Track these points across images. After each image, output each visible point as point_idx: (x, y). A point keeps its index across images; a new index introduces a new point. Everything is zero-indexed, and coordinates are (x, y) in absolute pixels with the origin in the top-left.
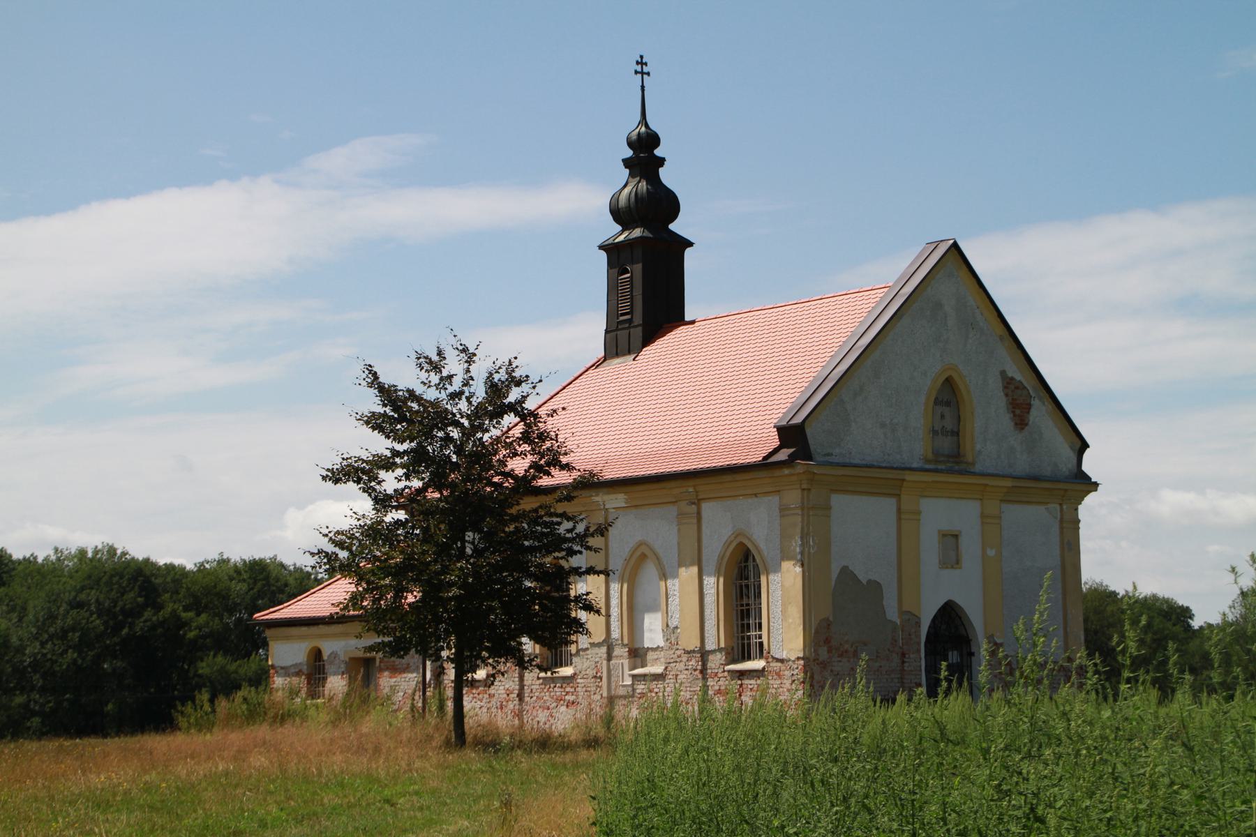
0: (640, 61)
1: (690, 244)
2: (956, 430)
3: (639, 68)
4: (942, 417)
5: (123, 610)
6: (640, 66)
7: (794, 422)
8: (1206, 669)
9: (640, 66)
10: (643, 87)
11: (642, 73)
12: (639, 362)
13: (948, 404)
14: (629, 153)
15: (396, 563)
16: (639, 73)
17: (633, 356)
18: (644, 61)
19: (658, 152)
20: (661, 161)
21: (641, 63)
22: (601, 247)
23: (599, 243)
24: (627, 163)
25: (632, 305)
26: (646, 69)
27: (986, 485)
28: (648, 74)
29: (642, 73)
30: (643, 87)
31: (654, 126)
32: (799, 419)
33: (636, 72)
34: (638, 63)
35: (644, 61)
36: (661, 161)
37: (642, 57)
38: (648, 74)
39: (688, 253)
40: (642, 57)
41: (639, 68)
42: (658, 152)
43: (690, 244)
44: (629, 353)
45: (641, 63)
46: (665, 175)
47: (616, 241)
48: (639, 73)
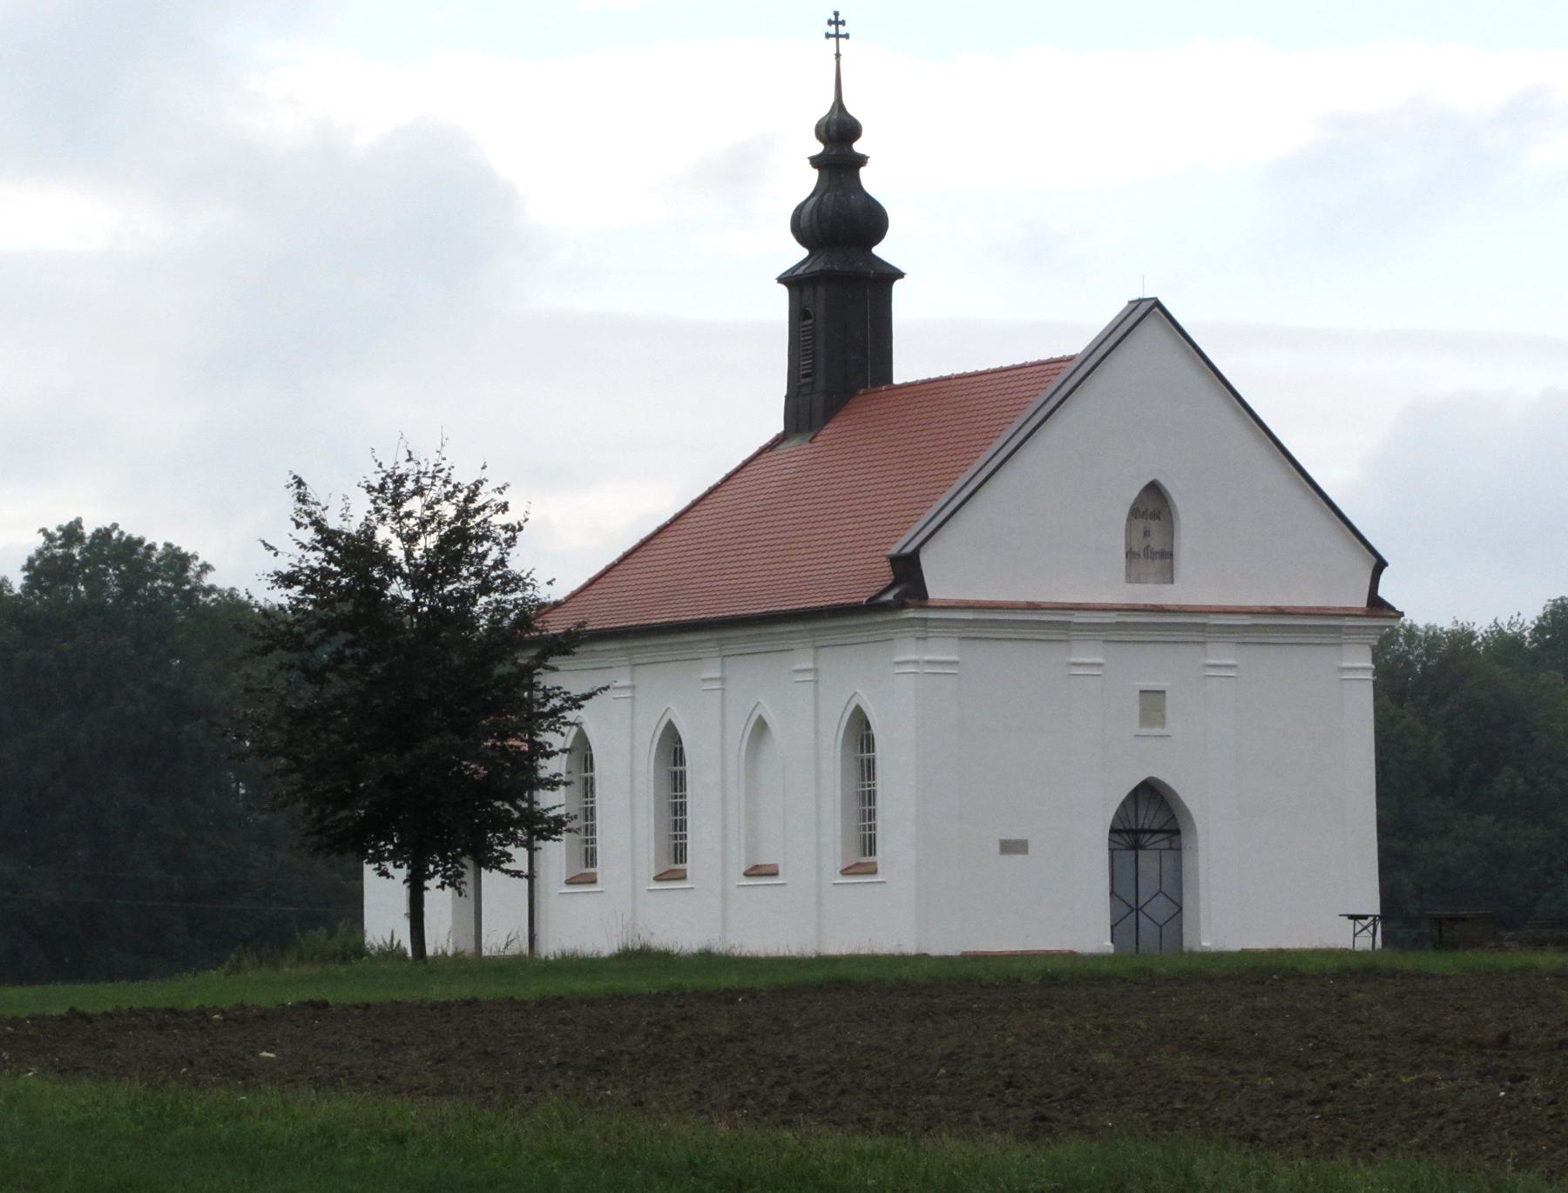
0: (833, 19)
1: (900, 275)
2: (1167, 549)
3: (832, 30)
4: (1146, 533)
5: (503, 607)
6: (833, 26)
7: (904, 551)
8: (185, 568)
9: (833, 26)
10: (838, 55)
11: (837, 36)
12: (817, 444)
13: (1155, 516)
14: (818, 148)
15: (542, 824)
16: (832, 36)
17: (810, 435)
18: (840, 19)
19: (858, 147)
20: (861, 160)
21: (836, 22)
22: (781, 280)
23: (779, 274)
24: (816, 162)
25: (813, 365)
26: (842, 30)
27: (926, 619)
28: (847, 36)
29: (837, 36)
30: (838, 55)
31: (853, 108)
32: (909, 549)
33: (828, 36)
34: (830, 23)
35: (840, 19)
36: (861, 160)
37: (836, 14)
38: (847, 36)
39: (898, 287)
40: (836, 14)
41: (832, 30)
42: (858, 147)
43: (900, 275)
44: (810, 429)
45: (836, 22)
46: (869, 179)
47: (796, 273)
48: (832, 36)
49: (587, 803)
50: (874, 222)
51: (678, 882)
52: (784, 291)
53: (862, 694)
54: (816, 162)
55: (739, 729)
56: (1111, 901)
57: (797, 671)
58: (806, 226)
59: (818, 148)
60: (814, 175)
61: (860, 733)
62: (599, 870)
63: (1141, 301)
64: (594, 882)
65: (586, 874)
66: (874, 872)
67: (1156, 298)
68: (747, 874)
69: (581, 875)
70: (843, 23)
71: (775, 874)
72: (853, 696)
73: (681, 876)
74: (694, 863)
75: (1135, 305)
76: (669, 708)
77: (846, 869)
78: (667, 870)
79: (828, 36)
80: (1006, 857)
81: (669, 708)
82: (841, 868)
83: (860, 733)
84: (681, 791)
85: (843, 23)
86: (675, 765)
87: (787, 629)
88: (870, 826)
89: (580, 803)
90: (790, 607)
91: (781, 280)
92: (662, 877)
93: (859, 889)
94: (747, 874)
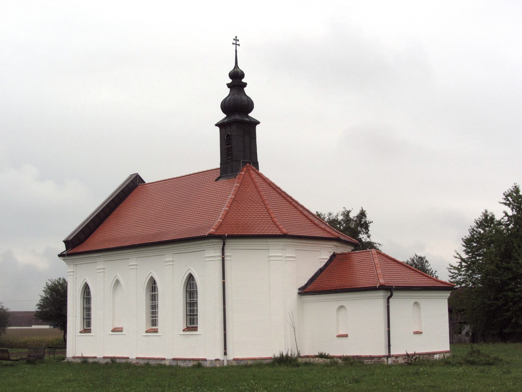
1: (258, 123)
3: (234, 42)
6: (235, 41)
9: (235, 41)
11: (236, 44)
18: (237, 39)
20: (245, 85)
21: (236, 40)
22: (216, 125)
24: (229, 85)
26: (238, 43)
29: (236, 44)
33: (233, 44)
34: (234, 40)
35: (237, 39)
36: (245, 85)
37: (236, 37)
38: (239, 45)
39: (258, 127)
40: (236, 37)
41: (234, 42)
43: (258, 123)
45: (236, 40)
46: (247, 90)
49: (153, 303)
50: (249, 106)
51: (155, 333)
52: (218, 129)
53: (119, 276)
54: (229, 85)
55: (110, 283)
56: (450, 346)
57: (97, 269)
58: (226, 107)
59: (230, 81)
60: (228, 90)
61: (152, 285)
62: (93, 327)
63: (133, 175)
64: (157, 332)
65: (153, 329)
66: (90, 332)
67: (137, 173)
68: (112, 331)
69: (151, 329)
70: (238, 40)
71: (122, 331)
72: (150, 273)
73: (156, 331)
74: (160, 326)
75: (131, 175)
76: (85, 279)
77: (81, 332)
78: (149, 329)
79: (233, 44)
80: (122, 327)
81: (85, 279)
82: (183, 329)
83: (152, 285)
84: (89, 304)
85: (238, 40)
86: (153, 292)
87: (273, 241)
88: (153, 318)
89: (150, 304)
90: (115, 246)
91: (216, 125)
92: (82, 332)
93: (192, 337)
94: (112, 331)
